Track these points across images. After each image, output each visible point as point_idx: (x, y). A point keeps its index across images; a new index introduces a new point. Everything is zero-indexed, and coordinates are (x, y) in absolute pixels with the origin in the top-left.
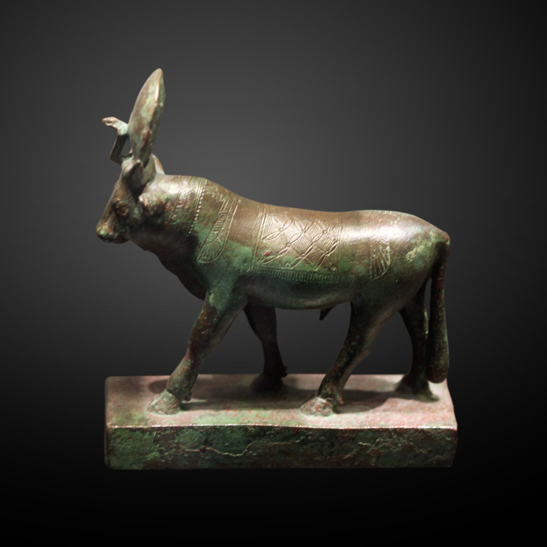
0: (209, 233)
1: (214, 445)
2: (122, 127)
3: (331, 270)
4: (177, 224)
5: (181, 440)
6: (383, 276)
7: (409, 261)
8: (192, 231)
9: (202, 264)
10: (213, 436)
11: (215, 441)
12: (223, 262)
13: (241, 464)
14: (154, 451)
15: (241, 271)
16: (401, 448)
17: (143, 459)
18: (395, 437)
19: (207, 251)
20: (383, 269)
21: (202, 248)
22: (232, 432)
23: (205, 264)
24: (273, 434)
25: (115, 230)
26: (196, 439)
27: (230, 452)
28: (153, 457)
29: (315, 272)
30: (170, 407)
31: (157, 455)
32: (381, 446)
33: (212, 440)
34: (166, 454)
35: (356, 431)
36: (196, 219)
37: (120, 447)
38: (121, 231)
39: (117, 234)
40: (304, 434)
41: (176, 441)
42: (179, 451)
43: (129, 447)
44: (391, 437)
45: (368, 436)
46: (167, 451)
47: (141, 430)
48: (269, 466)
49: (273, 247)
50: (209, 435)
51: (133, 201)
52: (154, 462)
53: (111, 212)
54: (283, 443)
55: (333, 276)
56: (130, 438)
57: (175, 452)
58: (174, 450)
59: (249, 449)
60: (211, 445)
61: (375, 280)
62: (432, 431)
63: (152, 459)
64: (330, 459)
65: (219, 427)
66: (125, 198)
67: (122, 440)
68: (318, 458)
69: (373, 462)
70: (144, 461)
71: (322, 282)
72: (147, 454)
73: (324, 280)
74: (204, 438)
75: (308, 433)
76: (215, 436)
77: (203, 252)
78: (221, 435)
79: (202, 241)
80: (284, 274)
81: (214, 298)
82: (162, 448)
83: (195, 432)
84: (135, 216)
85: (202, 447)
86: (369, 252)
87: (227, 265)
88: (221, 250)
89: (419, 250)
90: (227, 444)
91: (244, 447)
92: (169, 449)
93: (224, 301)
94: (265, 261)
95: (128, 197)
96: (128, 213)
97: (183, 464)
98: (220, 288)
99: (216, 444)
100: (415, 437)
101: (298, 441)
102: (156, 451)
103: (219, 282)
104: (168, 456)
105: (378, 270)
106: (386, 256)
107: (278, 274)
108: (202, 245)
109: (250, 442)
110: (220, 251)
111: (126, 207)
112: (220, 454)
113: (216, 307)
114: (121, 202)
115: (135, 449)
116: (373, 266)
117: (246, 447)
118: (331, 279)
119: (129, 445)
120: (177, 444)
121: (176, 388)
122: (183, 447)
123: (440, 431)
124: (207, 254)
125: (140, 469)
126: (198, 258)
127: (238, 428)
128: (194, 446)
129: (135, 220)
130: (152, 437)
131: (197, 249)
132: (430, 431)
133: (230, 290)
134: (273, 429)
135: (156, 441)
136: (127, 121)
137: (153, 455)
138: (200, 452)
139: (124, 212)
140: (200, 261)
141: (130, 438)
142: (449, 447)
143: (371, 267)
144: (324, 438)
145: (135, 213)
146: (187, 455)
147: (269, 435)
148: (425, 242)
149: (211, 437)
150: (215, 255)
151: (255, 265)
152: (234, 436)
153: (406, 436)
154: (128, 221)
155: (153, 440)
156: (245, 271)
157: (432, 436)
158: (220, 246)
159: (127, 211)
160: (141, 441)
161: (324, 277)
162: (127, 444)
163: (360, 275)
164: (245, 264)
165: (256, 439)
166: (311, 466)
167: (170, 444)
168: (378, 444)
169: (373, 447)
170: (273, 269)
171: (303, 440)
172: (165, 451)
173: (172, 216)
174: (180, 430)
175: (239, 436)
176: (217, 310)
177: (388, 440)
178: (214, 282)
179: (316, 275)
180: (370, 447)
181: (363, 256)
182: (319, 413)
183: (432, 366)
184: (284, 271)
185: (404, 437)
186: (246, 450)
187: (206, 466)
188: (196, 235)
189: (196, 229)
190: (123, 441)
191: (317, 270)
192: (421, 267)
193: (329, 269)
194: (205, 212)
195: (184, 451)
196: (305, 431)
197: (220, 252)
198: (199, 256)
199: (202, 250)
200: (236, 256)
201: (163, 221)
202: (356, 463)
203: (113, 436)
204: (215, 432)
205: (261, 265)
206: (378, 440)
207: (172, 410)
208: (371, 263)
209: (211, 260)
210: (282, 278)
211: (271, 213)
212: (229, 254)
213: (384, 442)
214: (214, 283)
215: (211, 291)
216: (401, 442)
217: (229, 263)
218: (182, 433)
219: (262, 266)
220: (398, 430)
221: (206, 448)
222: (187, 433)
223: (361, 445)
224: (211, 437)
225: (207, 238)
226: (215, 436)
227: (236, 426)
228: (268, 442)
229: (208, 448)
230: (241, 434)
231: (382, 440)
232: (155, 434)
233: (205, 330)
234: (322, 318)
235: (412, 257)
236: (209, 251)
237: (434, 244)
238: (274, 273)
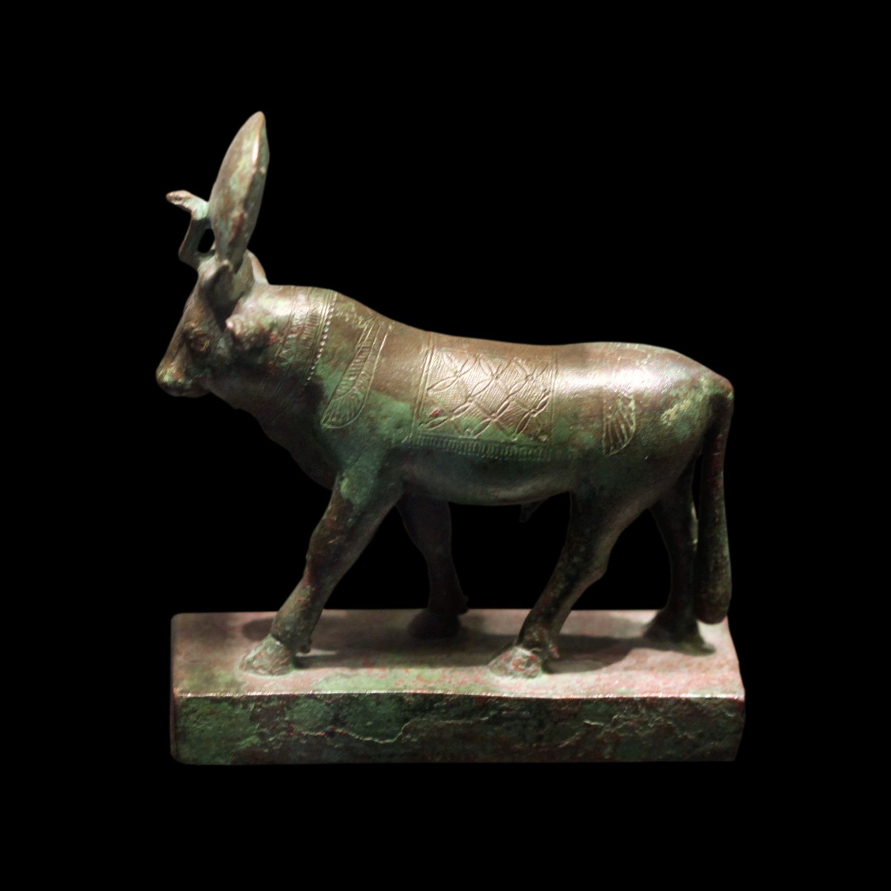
0: (341, 380)
2: (198, 207)
3: (540, 441)
4: (288, 364)
5: (295, 717)
6: (623, 449)
7: (666, 424)
8: (313, 376)
9: (328, 430)
10: (348, 711)
11: (349, 719)
12: (363, 427)
13: (392, 755)
14: (251, 735)
15: (393, 442)
16: (653, 730)
17: (233, 747)
18: (643, 711)
19: (338, 408)
21: (328, 404)
22: (378, 704)
23: (334, 430)
24: (445, 707)
25: (187, 374)
26: (319, 715)
27: (374, 736)
28: (249, 745)
29: (513, 444)
30: (277, 663)
31: (255, 742)
32: (620, 727)
33: (345, 717)
34: (271, 739)
35: (580, 703)
36: (319, 356)
37: (195, 727)
38: (197, 376)
39: (190, 382)
40: (495, 707)
41: (287, 719)
42: (292, 734)
43: (210, 728)
44: (636, 712)
45: (600, 710)
46: (272, 735)
47: (230, 701)
48: (438, 760)
49: (444, 402)
50: (341, 708)
51: (217, 327)
52: (251, 751)
53: (180, 346)
54: (460, 722)
55: (542, 449)
56: (212, 713)
57: (285, 736)
58: (284, 733)
59: (406, 732)
60: (343, 725)
61: (611, 456)
62: (704, 702)
63: (247, 748)
64: (538, 747)
65: (356, 696)
66: (203, 323)
67: (198, 717)
68: (518, 746)
69: (607, 754)
70: (234, 751)
71: (524, 460)
72: (239, 739)
73: (527, 456)
74: (332, 714)
75: (501, 706)
76: (351, 710)
77: (330, 411)
78: (360, 709)
79: (328, 393)
80: (463, 446)
81: (348, 486)
82: (265, 730)
83: (317, 703)
84: (220, 352)
85: (329, 728)
86: (602, 410)
87: (370, 431)
88: (360, 408)
89: (682, 407)
90: (369, 723)
91: (397, 729)
92: (275, 731)
93: (364, 490)
94: (432, 426)
95: (208, 320)
96: (209, 347)
97: (298, 756)
98: (359, 470)
99: (352, 723)
100: (675, 712)
101: (486, 718)
102: (254, 735)
103: (357, 460)
104: (273, 743)
105: (616, 439)
106: (629, 417)
107: (453, 446)
108: (329, 399)
109: (407, 720)
110: (358, 408)
111: (205, 338)
112: (358, 739)
113: (352, 500)
114: (196, 330)
115: (221, 732)
117: (400, 729)
118: (540, 454)
120: (288, 722)
121: (287, 632)
122: (297, 728)
123: (716, 702)
124: (337, 413)
125: (229, 763)
126: (323, 421)
127: (388, 697)
128: (316, 726)
129: (220, 358)
130: (248, 712)
131: (322, 405)
132: (701, 702)
133: (375, 472)
134: (444, 699)
135: (254, 718)
136: (206, 197)
137: (250, 741)
138: (326, 736)
139: (203, 345)
140: (326, 426)
141: (212, 713)
142: (732, 729)
143: (604, 435)
144: (528, 713)
145: (220, 348)
146: (304, 742)
147: (439, 708)
148: (692, 393)
149: (344, 712)
150: (350, 415)
152: (382, 710)
153: (661, 710)
154: (209, 360)
155: (248, 717)
156: (398, 442)
157: (703, 710)
158: (359, 401)
159: (207, 343)
160: (230, 718)
161: (528, 451)
162: (206, 722)
163: (587, 448)
164: (399, 430)
165: (416, 716)
166: (507, 760)
167: (277, 723)
168: (616, 723)
169: (608, 729)
170: (445, 438)
171: (494, 717)
172: (270, 734)
173: (279, 353)
174: (294, 701)
175: (389, 709)
176: (353, 505)
177: (632, 716)
178: (348, 459)
179: (515, 448)
180: (602, 728)
182: (519, 673)
183: (704, 596)
184: (462, 442)
185: (658, 711)
186: (401, 733)
187: (335, 758)
188: (319, 382)
189: (319, 372)
190: (201, 718)
191: (516, 439)
192: (685, 435)
193: (536, 438)
194: (334, 345)
195: (300, 734)
196: (497, 702)
197: (359, 411)
198: (325, 417)
199: (330, 407)
200: (385, 417)
201: (266, 360)
202: (580, 755)
204: (350, 703)
205: (424, 431)
206: (615, 717)
207: (280, 668)
208: (604, 429)
209: (343, 423)
210: (460, 453)
211: (441, 348)
212: (372, 413)
213: (626, 720)
214: (349, 461)
215: (344, 475)
216: (654, 719)
217: (373, 429)
218: (297, 705)
219: (428, 433)
220: (648, 700)
221: (335, 729)
222: (304, 705)
223: (589, 725)
224: (344, 712)
225: (337, 388)
226: (351, 710)
227: (384, 694)
228: (436, 719)
229: (339, 730)
230: (393, 707)
231: (622, 716)
232: (252, 706)
233: (333, 538)
235: (671, 419)
236: (340, 409)
237: (707, 398)
238: (447, 444)
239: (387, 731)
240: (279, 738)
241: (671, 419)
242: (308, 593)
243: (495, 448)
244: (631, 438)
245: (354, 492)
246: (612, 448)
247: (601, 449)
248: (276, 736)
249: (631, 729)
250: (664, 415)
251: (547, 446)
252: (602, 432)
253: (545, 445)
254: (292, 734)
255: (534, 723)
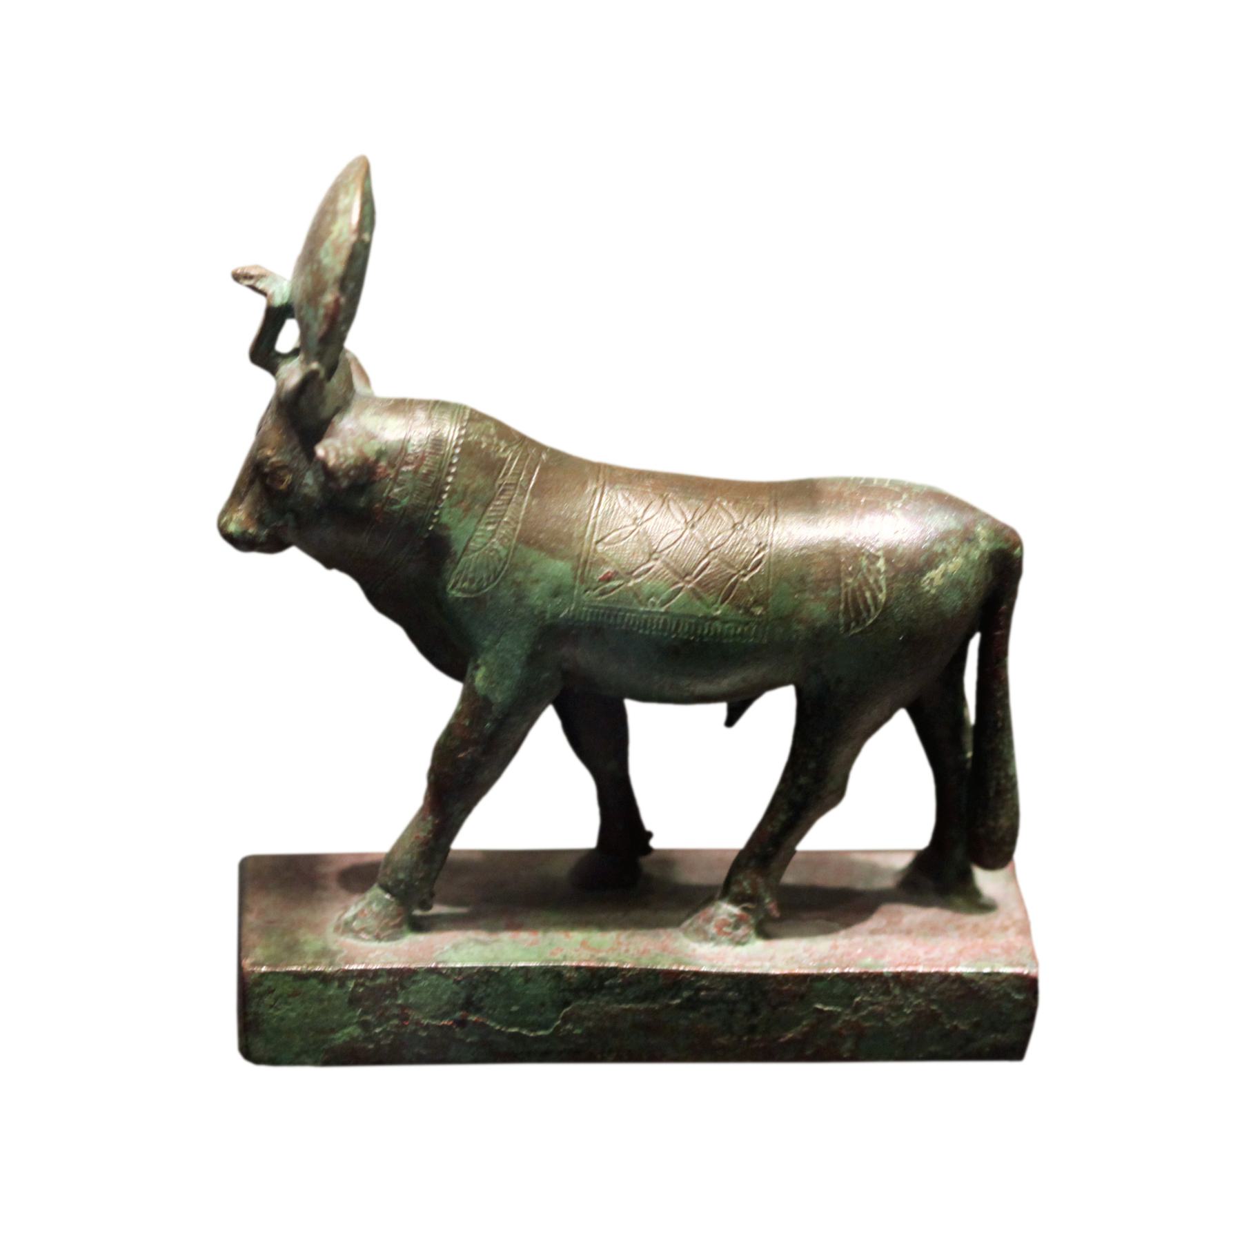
0: (475, 530)
1: (486, 1010)
4: (401, 508)
5: (412, 1000)
7: (928, 592)
8: (437, 524)
9: (458, 599)
10: (485, 991)
11: (487, 1002)
12: (506, 595)
14: (350, 1025)
15: (548, 616)
16: (911, 1018)
17: (324, 1042)
18: (897, 991)
19: (471, 569)
20: (869, 611)
21: (458, 563)
22: (527, 981)
23: (465, 600)
24: (620, 985)
26: (445, 997)
27: (522, 1026)
28: (347, 1038)
29: (715, 618)
30: (387, 924)
31: (356, 1034)
32: (864, 1013)
33: (481, 999)
34: (377, 1030)
38: (275, 524)
39: (265, 532)
40: (689, 985)
41: (400, 1002)
42: (407, 1024)
43: (293, 1015)
44: (887, 992)
45: (836, 990)
46: (379, 1025)
47: (321, 977)
49: (619, 560)
50: (475, 988)
51: (302, 455)
54: (642, 1006)
55: (756, 626)
56: (295, 994)
57: (397, 1026)
58: (395, 1022)
59: (565, 1020)
60: (478, 1010)
61: (852, 636)
62: (981, 979)
63: (345, 1042)
64: (750, 1041)
65: (497, 970)
66: (283, 450)
67: (276, 1000)
70: (326, 1046)
71: (731, 641)
72: (333, 1031)
73: (735, 635)
74: (463, 995)
75: (698, 984)
76: (489, 990)
77: (460, 572)
78: (502, 988)
79: (458, 547)
80: (646, 621)
81: (485, 678)
82: (369, 1018)
83: (442, 980)
84: (306, 490)
85: (458, 1015)
86: (839, 571)
87: (516, 601)
88: (502, 569)
89: (951, 567)
90: (514, 1008)
91: (553, 1016)
92: (383, 1019)
93: (508, 682)
94: (602, 593)
95: (290, 447)
96: (291, 483)
98: (501, 655)
99: (490, 1008)
100: (941, 993)
101: (677, 1001)
102: (354, 1024)
103: (497, 641)
104: (381, 1036)
105: (858, 613)
107: (631, 622)
108: (459, 556)
109: (567, 1004)
110: (499, 569)
111: (286, 471)
112: (499, 1030)
113: (491, 697)
114: (274, 459)
115: (307, 1021)
116: (846, 604)
117: (558, 1016)
118: (752, 633)
119: (292, 1010)
120: (402, 1007)
121: (401, 881)
122: (414, 1015)
123: (999, 978)
124: (470, 576)
126: (450, 586)
127: (541, 971)
128: (440, 1012)
129: (307, 499)
130: (345, 993)
131: (448, 564)
132: (977, 979)
133: (523, 658)
134: (619, 975)
135: (354, 1001)
137: (348, 1033)
138: (454, 1027)
139: (282, 481)
140: (455, 593)
141: (295, 994)
143: (842, 607)
144: (737, 994)
145: (306, 485)
146: (424, 1034)
147: (611, 987)
148: (965, 548)
149: (480, 993)
150: (488, 578)
151: (578, 603)
152: (532, 989)
153: (922, 989)
154: (291, 501)
155: (346, 1000)
156: (555, 616)
157: (980, 989)
158: (500, 560)
159: (289, 478)
160: (321, 1001)
161: (736, 629)
162: (288, 1007)
163: (818, 624)
164: (556, 600)
165: (580, 998)
167: (387, 1008)
168: (858, 1008)
169: (848, 1016)
170: (620, 610)
171: (689, 999)
172: (376, 1023)
173: (390, 491)
174: (410, 977)
176: (492, 705)
177: (881, 998)
178: (485, 639)
179: (717, 624)
180: (839, 1014)
181: (824, 581)
182: (724, 938)
183: (982, 831)
184: (644, 616)
185: (917, 992)
186: (558, 1022)
188: (445, 533)
189: (445, 519)
190: (280, 1000)
191: (719, 612)
192: (956, 607)
193: (747, 611)
194: (466, 481)
195: (418, 1023)
196: (692, 979)
197: (500, 572)
198: (452, 581)
199: (459, 567)
200: (537, 581)
201: (371, 502)
203: (257, 990)
204: (488, 980)
205: (592, 601)
206: (857, 999)
207: (390, 931)
208: (843, 597)
209: (479, 590)
210: (641, 631)
212: (519, 576)
213: (872, 1004)
214: (486, 643)
215: (479, 662)
216: (911, 1003)
217: (520, 598)
218: (414, 982)
219: (596, 604)
220: (903, 975)
221: (467, 1016)
222: (424, 983)
223: (821, 1011)
224: (480, 993)
225: (469, 540)
226: (489, 990)
227: (535, 968)
228: (608, 1003)
229: (473, 1018)
230: (548, 986)
231: (866, 998)
232: (351, 985)
233: (465, 750)
234: (730, 722)
235: (935, 583)
236: (475, 571)
237: (986, 555)
238: (623, 619)
239: (540, 1019)
240: (388, 1029)
241: (935, 583)
242: (429, 826)
243: (690, 624)
244: (880, 611)
245: (493, 686)
246: (853, 624)
247: (837, 626)
248: (385, 1026)
249: (880, 1016)
250: (925, 578)
251: (762, 621)
252: (839, 602)
253: (760, 620)
254: (407, 1024)
255: (745, 1007)
